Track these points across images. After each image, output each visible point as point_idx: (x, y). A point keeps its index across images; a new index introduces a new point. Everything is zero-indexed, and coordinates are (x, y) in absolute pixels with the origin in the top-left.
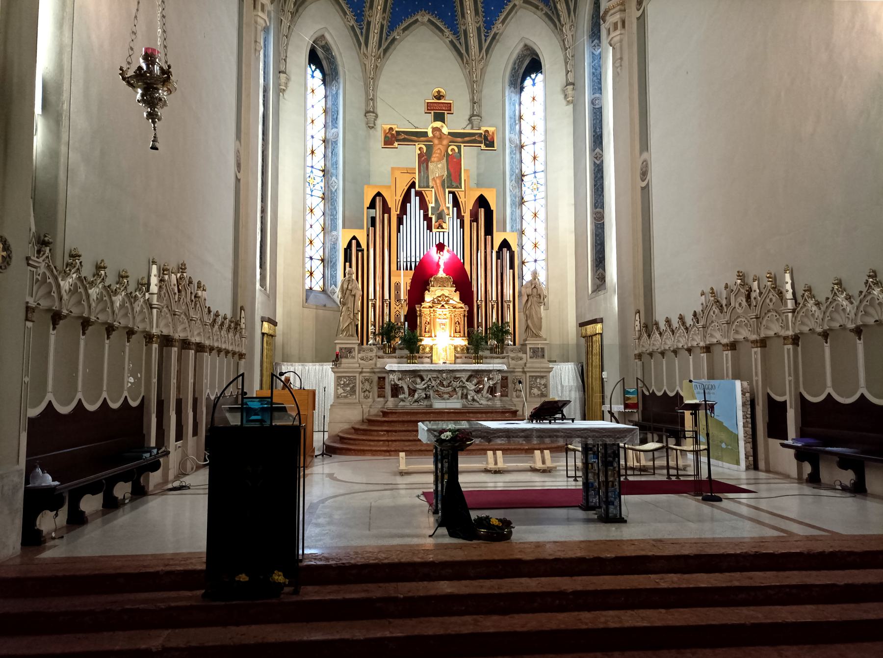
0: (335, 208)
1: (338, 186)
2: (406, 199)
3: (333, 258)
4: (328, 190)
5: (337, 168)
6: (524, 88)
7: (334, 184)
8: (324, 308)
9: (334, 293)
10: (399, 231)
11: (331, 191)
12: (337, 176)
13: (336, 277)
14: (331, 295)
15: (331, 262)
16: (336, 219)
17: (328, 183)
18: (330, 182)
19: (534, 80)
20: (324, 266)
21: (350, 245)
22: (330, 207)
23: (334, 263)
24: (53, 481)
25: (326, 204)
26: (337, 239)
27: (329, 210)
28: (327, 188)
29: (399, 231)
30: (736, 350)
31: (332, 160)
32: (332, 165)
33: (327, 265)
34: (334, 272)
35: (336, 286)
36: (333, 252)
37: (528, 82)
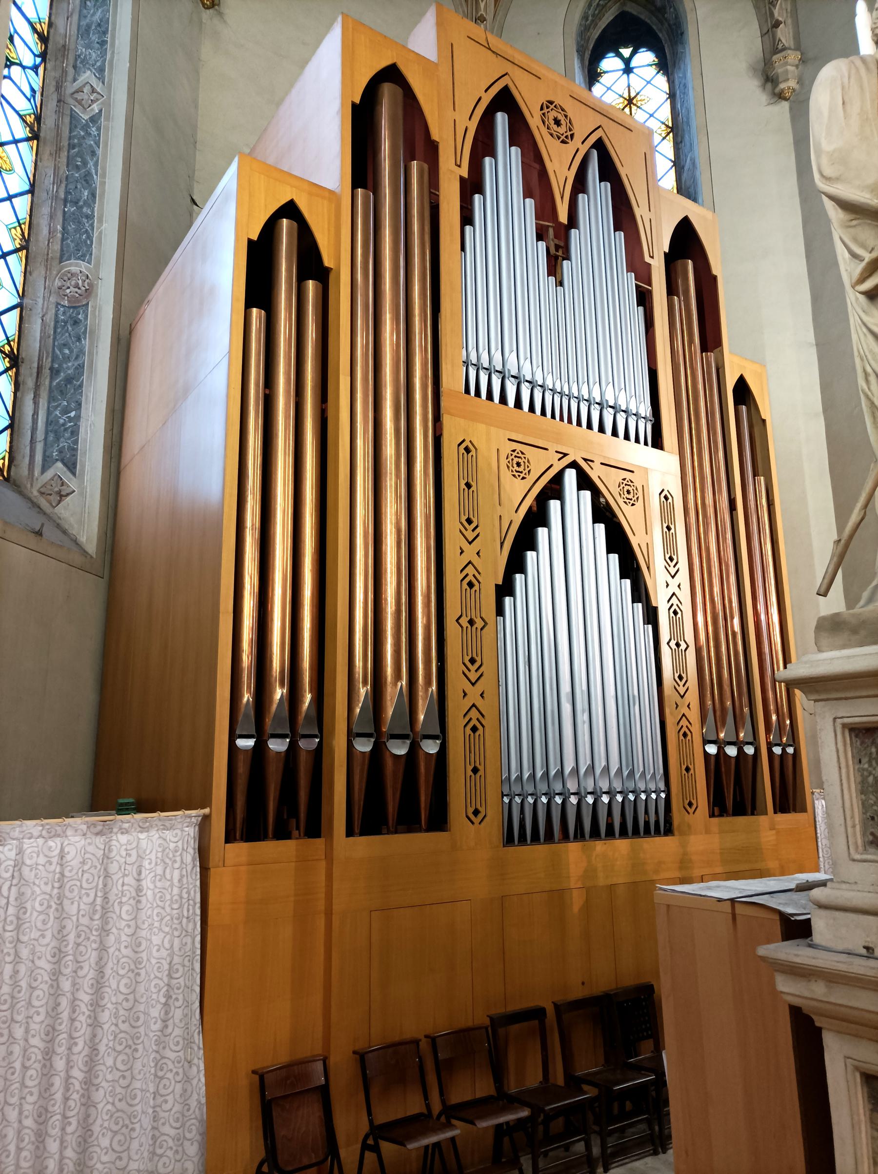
0: (87, 179)
1: (108, 104)
2: (487, 124)
3: (67, 359)
4: (59, 112)
5: (103, 43)
6: (600, 75)
7: (85, 96)
8: (32, 541)
9: (62, 496)
10: (467, 219)
11: (73, 117)
12: (101, 70)
13: (75, 432)
14: (43, 503)
15: (55, 373)
16: (90, 217)
17: (59, 87)
18: (70, 88)
19: (627, 62)
20: (17, 386)
21: (270, 228)
22: (63, 170)
23: (69, 380)
24: (767, 814)
25: (46, 156)
26: (89, 292)
27: (57, 181)
28: (52, 105)
29: (467, 219)
30: (710, 817)
31: (81, 16)
32: (84, 32)
33: (30, 383)
34: (66, 411)
35: (72, 467)
36: (64, 338)
37: (610, 63)
